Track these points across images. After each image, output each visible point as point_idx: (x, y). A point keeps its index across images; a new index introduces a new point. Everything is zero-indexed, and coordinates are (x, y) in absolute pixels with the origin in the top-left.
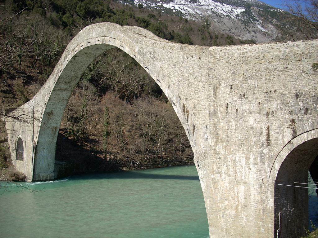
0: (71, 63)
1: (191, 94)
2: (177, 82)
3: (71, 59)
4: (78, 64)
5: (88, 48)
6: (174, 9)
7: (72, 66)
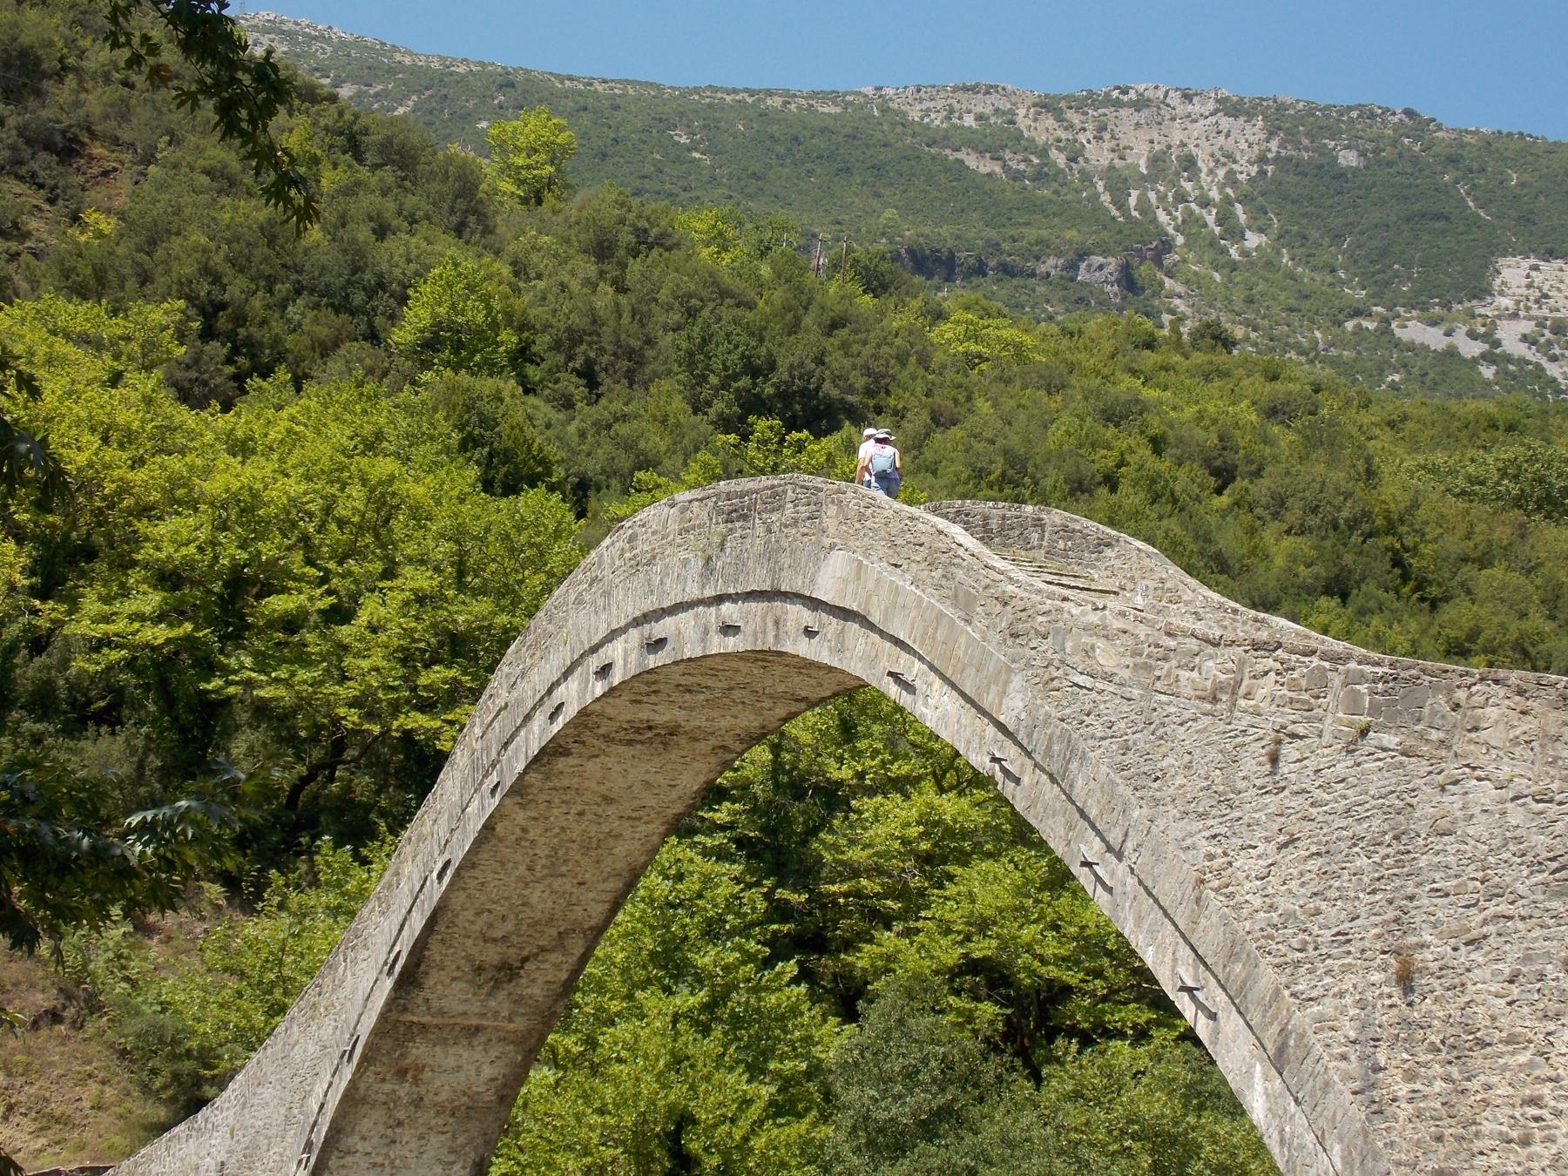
0: (523, 806)
1: (1487, 1127)
2: (1352, 1012)
3: (522, 776)
4: (581, 814)
5: (645, 684)
6: (1487, 358)
7: (531, 836)
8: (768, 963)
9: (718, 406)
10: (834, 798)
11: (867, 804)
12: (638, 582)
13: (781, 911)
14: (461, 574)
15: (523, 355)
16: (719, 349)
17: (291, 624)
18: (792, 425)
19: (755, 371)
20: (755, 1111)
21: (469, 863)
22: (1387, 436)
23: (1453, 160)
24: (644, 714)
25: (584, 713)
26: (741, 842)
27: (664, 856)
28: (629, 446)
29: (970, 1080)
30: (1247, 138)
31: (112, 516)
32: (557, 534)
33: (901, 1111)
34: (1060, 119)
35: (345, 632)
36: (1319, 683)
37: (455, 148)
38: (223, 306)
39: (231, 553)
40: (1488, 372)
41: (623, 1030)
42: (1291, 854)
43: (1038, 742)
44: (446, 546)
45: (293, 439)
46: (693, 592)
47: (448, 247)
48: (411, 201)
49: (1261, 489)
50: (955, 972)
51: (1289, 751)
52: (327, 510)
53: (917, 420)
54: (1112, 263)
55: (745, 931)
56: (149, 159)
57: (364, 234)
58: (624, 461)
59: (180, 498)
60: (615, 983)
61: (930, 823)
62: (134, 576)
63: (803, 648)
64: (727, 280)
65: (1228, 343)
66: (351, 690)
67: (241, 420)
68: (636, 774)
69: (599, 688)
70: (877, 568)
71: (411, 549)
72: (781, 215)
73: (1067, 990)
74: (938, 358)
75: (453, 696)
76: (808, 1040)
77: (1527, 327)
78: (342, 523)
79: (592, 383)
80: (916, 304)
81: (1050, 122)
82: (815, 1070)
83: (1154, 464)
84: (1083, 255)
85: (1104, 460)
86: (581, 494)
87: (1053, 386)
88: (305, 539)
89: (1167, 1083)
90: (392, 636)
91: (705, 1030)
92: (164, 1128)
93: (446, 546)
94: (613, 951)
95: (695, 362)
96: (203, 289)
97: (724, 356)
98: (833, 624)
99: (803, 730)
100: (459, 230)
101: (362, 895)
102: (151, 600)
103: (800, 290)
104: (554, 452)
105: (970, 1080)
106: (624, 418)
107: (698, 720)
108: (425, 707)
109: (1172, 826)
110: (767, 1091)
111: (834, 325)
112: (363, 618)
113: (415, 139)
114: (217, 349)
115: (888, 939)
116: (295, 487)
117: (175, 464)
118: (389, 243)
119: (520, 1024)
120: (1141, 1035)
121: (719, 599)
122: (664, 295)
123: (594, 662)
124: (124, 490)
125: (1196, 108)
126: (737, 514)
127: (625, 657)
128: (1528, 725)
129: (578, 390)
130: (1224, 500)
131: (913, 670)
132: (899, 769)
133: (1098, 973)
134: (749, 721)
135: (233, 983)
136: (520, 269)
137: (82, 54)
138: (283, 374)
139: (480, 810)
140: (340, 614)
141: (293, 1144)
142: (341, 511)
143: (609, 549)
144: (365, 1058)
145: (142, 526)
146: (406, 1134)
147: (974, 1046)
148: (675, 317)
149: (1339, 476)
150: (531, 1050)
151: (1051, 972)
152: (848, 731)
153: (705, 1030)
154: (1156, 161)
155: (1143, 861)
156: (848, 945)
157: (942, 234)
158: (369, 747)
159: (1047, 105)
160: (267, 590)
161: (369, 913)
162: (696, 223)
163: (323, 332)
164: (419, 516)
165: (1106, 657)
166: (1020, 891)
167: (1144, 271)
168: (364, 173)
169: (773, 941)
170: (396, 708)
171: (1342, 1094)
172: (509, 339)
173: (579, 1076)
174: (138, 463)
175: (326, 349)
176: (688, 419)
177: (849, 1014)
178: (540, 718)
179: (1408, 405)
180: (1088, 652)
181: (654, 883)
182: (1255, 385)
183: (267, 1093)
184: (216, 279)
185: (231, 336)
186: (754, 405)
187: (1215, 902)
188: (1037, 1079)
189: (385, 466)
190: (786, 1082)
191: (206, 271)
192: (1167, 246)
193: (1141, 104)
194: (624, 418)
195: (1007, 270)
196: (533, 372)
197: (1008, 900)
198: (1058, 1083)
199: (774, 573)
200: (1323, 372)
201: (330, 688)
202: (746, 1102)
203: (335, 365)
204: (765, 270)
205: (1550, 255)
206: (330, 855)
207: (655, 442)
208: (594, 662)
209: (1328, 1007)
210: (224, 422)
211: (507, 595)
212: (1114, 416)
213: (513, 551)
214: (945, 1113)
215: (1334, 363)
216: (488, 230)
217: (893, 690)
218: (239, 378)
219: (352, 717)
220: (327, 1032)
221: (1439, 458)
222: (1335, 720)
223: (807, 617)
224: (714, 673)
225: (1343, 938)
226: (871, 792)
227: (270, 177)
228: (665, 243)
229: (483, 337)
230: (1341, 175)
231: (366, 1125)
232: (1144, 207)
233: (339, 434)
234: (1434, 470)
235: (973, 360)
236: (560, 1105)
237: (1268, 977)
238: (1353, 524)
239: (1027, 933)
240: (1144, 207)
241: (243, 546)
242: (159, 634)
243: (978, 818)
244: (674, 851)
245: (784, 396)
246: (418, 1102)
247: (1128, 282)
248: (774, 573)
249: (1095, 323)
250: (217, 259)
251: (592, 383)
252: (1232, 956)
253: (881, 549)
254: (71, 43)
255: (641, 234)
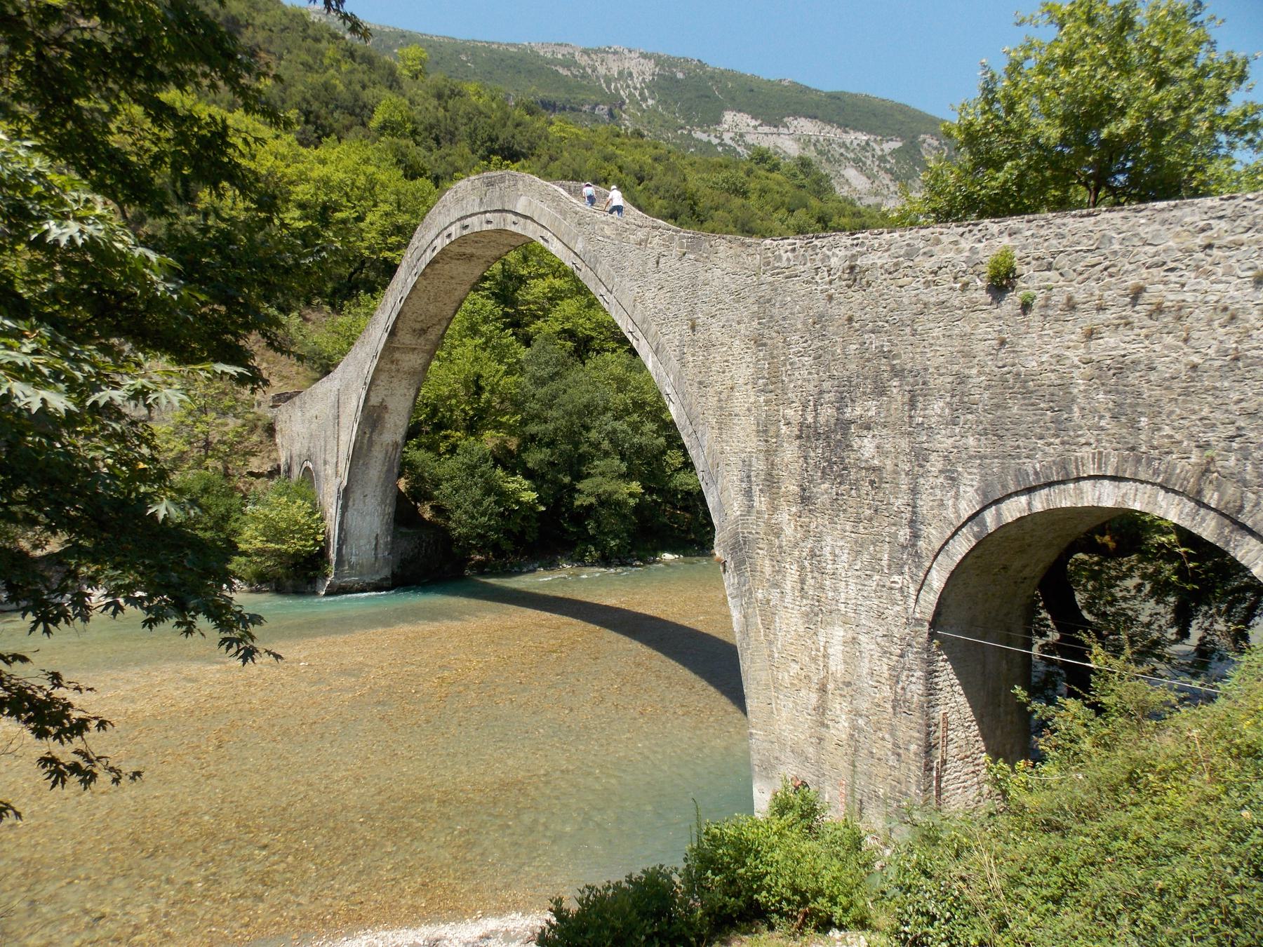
5: (462, 240)
8: (503, 330)
9: (480, 152)
10: (522, 280)
11: (532, 282)
12: (459, 206)
13: (506, 315)
14: (399, 206)
15: (414, 132)
16: (480, 132)
17: (344, 221)
18: (505, 158)
19: (492, 140)
20: (501, 373)
21: (409, 298)
22: (689, 168)
23: (712, 78)
24: (462, 250)
25: (443, 249)
26: (493, 294)
27: (470, 297)
28: (452, 164)
29: (564, 364)
30: (649, 67)
31: (281, 184)
32: (430, 194)
33: (544, 373)
34: (589, 56)
35: (362, 225)
36: (672, 238)
37: (387, 58)
38: (311, 112)
39: (322, 198)
40: (720, 149)
41: (459, 350)
42: (662, 291)
43: (587, 258)
44: (393, 197)
45: (339, 159)
46: (477, 210)
47: (387, 93)
48: (373, 76)
49: (652, 184)
50: (559, 333)
51: (662, 260)
52: (353, 184)
53: (545, 158)
54: (606, 108)
55: (496, 320)
56: (281, 58)
57: (358, 88)
58: (450, 170)
59: (303, 178)
60: (456, 336)
61: (551, 288)
62: (290, 205)
63: (513, 228)
64: (482, 108)
65: (642, 136)
66: (366, 244)
67: (321, 152)
68: (461, 269)
69: (448, 242)
70: (536, 202)
71: (382, 197)
72: (499, 86)
73: (593, 338)
74: (551, 137)
75: (399, 247)
76: (516, 353)
77: (732, 135)
78: (358, 188)
79: (438, 143)
80: (543, 119)
81: (586, 57)
82: (519, 361)
83: (619, 175)
84: (597, 105)
85: (604, 173)
86: (437, 180)
87: (588, 148)
88: (346, 194)
89: (621, 364)
90: (378, 226)
91: (484, 350)
92: (318, 380)
93: (393, 197)
94: (455, 326)
95: (472, 136)
96: (304, 106)
97: (482, 134)
98: (522, 220)
99: (513, 257)
100: (390, 87)
101: (375, 309)
102: (297, 213)
103: (505, 113)
104: (427, 166)
105: (564, 364)
106: (449, 155)
107: (479, 252)
108: (390, 250)
109: (627, 284)
110: (504, 368)
111: (518, 125)
112: (368, 220)
113: (373, 54)
114: (310, 127)
115: (540, 323)
116: (341, 175)
117: (300, 166)
118: (367, 91)
119: (428, 347)
120: (614, 351)
121: (485, 212)
122: (461, 113)
123: (446, 233)
124: (284, 175)
125: (633, 55)
126: (490, 184)
127: (455, 231)
128: (732, 252)
129: (433, 144)
130: (641, 188)
131: (548, 235)
132: (541, 271)
133: (601, 333)
134: (496, 253)
135: (336, 336)
136: (412, 102)
137: (254, 19)
138: (334, 137)
139: (411, 281)
140: (360, 219)
141: (360, 383)
142: (358, 184)
143: (448, 195)
144: (381, 358)
145: (291, 188)
146: (395, 380)
147: (566, 355)
148: (465, 121)
149: (675, 181)
150: (432, 356)
151: (588, 333)
152: (525, 259)
153: (484, 350)
154: (620, 73)
155: (618, 294)
156: (527, 325)
157: (552, 96)
158: (373, 263)
159: (585, 52)
160: (335, 210)
161: (378, 313)
162: (470, 88)
163: (346, 122)
164: (384, 186)
165: (608, 231)
166: (578, 309)
167: (616, 111)
168: (356, 66)
169: (504, 324)
170: (381, 250)
171: (674, 360)
172: (409, 126)
173: (447, 364)
174: (288, 166)
175: (348, 128)
176: (470, 156)
177: (528, 344)
178: (429, 251)
179: (696, 159)
180: (602, 229)
181: (466, 305)
182: (650, 150)
183: (351, 368)
184: (308, 103)
185: (315, 123)
186: (492, 151)
187: (639, 306)
188: (584, 363)
189: (371, 169)
190: (509, 365)
191: (304, 99)
192: (623, 103)
193: (615, 53)
194: (449, 155)
195: (572, 109)
196: (417, 138)
197: (575, 311)
198: (590, 364)
199: (503, 203)
200: (671, 147)
201: (358, 243)
202: (498, 371)
203: (351, 134)
204: (494, 105)
205: (740, 111)
206: (364, 297)
207: (460, 163)
208: (446, 233)
209: (671, 336)
210: (316, 152)
211: (415, 213)
212: (607, 159)
213: (416, 199)
214: (557, 374)
215: (674, 144)
216: (400, 88)
217: (542, 242)
218: (319, 138)
219: (366, 253)
220: (368, 349)
221: (705, 175)
222: (676, 251)
223: (514, 218)
224: (484, 237)
225: (676, 316)
226: (533, 278)
227: (349, 24)
228: (460, 94)
229: (401, 125)
230: (678, 81)
231: (382, 377)
232: (616, 89)
233: (356, 158)
234: (702, 179)
235: (562, 139)
236: (441, 372)
237: (654, 328)
238: (679, 196)
239: (581, 321)
240: (616, 89)
241: (326, 195)
242: (301, 224)
243: (566, 286)
244: (472, 295)
245: (502, 149)
246: (398, 371)
247: (611, 114)
248: (503, 203)
249: (601, 128)
250: (308, 96)
251: (438, 143)
252: (644, 322)
253: (537, 196)
254: (249, 14)
255: (452, 91)
